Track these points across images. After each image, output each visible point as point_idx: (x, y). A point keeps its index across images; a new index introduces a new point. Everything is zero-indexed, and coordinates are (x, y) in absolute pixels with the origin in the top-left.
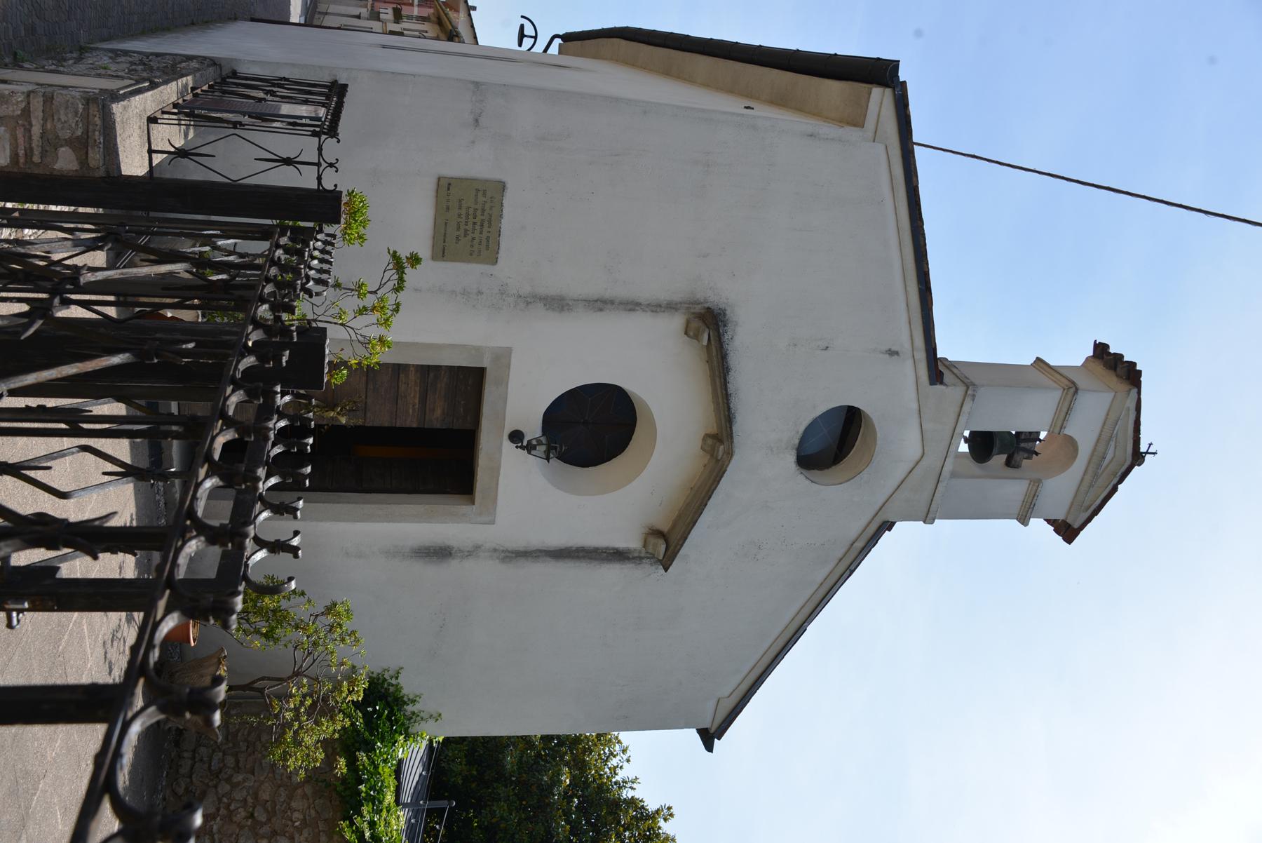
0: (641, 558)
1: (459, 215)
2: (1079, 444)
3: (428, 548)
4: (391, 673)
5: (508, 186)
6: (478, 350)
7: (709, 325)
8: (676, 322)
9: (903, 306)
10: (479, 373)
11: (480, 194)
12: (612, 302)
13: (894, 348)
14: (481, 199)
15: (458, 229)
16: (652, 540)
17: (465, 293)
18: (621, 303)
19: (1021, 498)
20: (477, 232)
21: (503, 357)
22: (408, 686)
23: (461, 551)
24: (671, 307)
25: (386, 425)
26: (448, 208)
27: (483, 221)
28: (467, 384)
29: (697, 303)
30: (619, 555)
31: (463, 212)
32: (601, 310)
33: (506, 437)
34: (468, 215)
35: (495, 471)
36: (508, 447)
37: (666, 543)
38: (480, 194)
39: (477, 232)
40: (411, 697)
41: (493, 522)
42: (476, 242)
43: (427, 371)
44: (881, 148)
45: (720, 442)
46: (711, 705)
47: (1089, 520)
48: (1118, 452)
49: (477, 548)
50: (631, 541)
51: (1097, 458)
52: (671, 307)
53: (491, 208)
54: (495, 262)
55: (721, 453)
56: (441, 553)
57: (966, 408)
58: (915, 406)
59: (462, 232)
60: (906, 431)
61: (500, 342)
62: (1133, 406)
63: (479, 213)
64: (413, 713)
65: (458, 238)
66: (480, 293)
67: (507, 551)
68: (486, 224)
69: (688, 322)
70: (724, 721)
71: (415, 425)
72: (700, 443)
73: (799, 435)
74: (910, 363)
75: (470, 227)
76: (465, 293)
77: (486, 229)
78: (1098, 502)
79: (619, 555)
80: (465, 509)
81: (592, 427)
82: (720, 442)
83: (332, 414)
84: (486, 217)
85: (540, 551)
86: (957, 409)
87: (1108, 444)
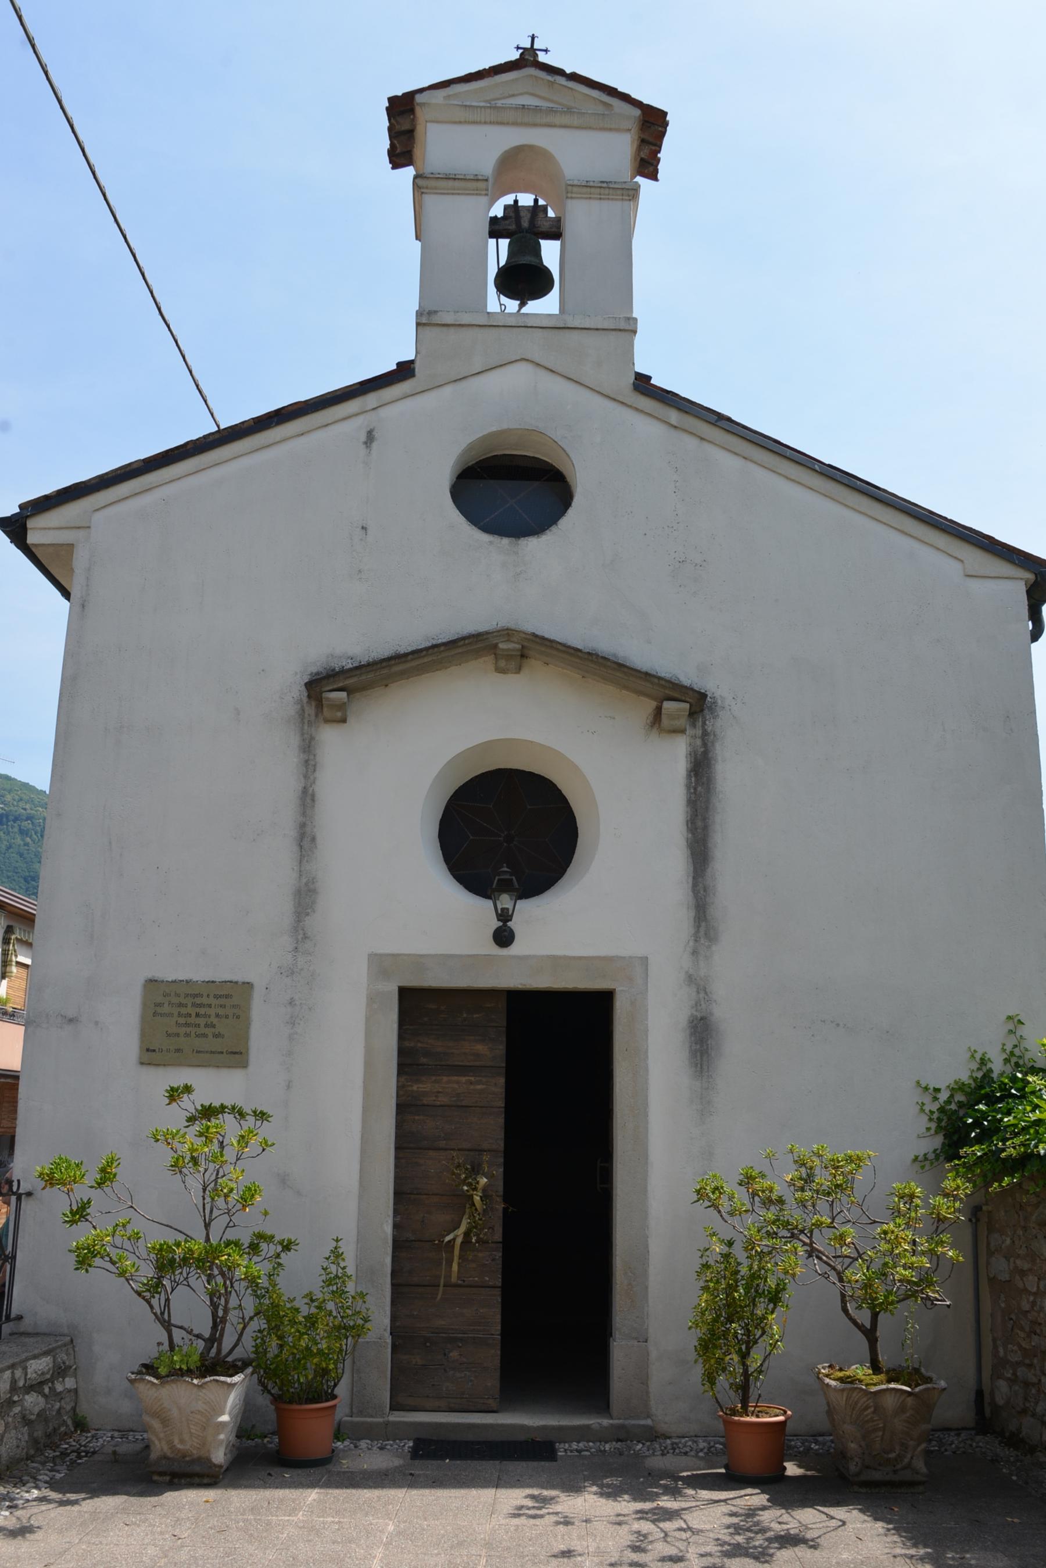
0: (705, 733)
1: (187, 1035)
2: (507, 147)
3: (693, 1054)
4: (927, 1099)
5: (150, 976)
6: (371, 999)
7: (334, 691)
8: (329, 736)
9: (302, 440)
10: (405, 994)
11: (159, 1010)
12: (303, 826)
13: (363, 437)
14: (166, 1009)
15: (205, 1035)
16: (665, 721)
17: (292, 1022)
18: (304, 814)
19: (595, 204)
20: (209, 1011)
21: (381, 964)
22: (951, 1070)
23: (697, 1004)
24: (308, 748)
25: (501, 1120)
26: (178, 1050)
27: (194, 1005)
28: (426, 1014)
29: (302, 713)
30: (700, 768)
31: (183, 1030)
32: (313, 839)
33: (504, 952)
34: (187, 1025)
35: (557, 962)
36: (516, 949)
37: (680, 706)
38: (159, 1010)
39: (209, 1011)
40: (975, 1066)
41: (644, 960)
42: (221, 1012)
43: (409, 1063)
44: (98, 517)
45: (508, 650)
46: (975, 586)
47: (626, 98)
48: (522, 91)
49: (690, 979)
50: (674, 755)
51: (527, 117)
52: (308, 748)
53: (178, 995)
54: (249, 986)
55: (511, 646)
56: (702, 1037)
57: (449, 319)
58: (448, 390)
59: (209, 1031)
60: (504, 401)
61: (360, 971)
62: (441, 93)
63: (184, 1011)
64: (1007, 1061)
65: (217, 1036)
66: (291, 1002)
67: (697, 932)
68: (198, 1001)
69: (327, 721)
70: (1011, 561)
71: (502, 1081)
72: (512, 678)
73: (495, 539)
74: (383, 412)
75: (202, 1021)
76: (292, 1022)
77: (204, 1000)
78: (595, 93)
79: (700, 768)
80: (621, 1007)
81: (508, 831)
82: (508, 650)
83: (477, 1198)
84: (189, 1001)
85: (695, 885)
86: (452, 330)
87: (503, 108)
